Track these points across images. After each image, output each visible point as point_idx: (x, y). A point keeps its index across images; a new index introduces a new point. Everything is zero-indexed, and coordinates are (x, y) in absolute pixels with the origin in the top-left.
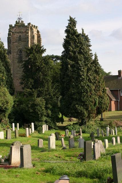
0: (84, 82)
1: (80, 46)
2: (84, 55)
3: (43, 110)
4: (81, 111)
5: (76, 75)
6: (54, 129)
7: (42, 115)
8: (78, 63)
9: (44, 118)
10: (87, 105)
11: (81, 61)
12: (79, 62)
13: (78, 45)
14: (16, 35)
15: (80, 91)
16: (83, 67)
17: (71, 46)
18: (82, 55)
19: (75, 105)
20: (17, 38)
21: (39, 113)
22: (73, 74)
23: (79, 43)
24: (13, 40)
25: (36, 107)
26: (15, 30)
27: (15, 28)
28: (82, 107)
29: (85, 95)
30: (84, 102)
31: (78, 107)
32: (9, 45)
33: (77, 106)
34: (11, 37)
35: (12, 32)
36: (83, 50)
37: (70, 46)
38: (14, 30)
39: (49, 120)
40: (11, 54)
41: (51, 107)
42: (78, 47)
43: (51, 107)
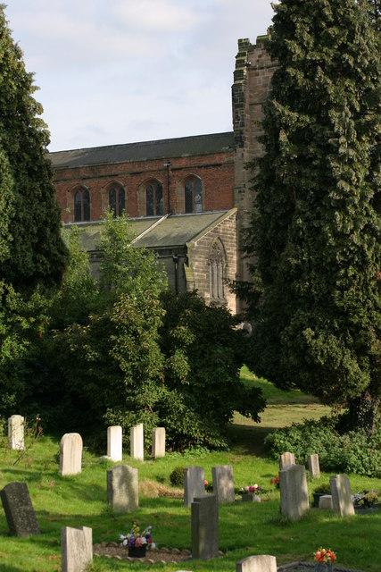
0: (352, 211)
1: (338, 37)
2: (363, 83)
3: (144, 352)
4: (330, 359)
5: (313, 178)
6: (203, 446)
7: (140, 377)
8: (327, 122)
9: (152, 394)
10: (358, 327)
11: (340, 108)
12: (333, 113)
13: (333, 31)
14: (261, 77)
15: (329, 260)
16: (348, 136)
17: (296, 39)
18: (347, 83)
19: (302, 327)
20: (265, 86)
21: (124, 365)
22: (299, 175)
23: (336, 23)
24: (251, 97)
25: (113, 337)
26: (260, 56)
27: (258, 52)
28: (333, 340)
29: (354, 276)
30: (343, 313)
31: (315, 337)
32: (237, 113)
33: (308, 332)
34: (245, 83)
35: (248, 65)
36: (355, 55)
37: (293, 38)
38: (254, 60)
39: (177, 400)
40: (242, 146)
41: (190, 338)
42: (330, 41)
43: (190, 338)
